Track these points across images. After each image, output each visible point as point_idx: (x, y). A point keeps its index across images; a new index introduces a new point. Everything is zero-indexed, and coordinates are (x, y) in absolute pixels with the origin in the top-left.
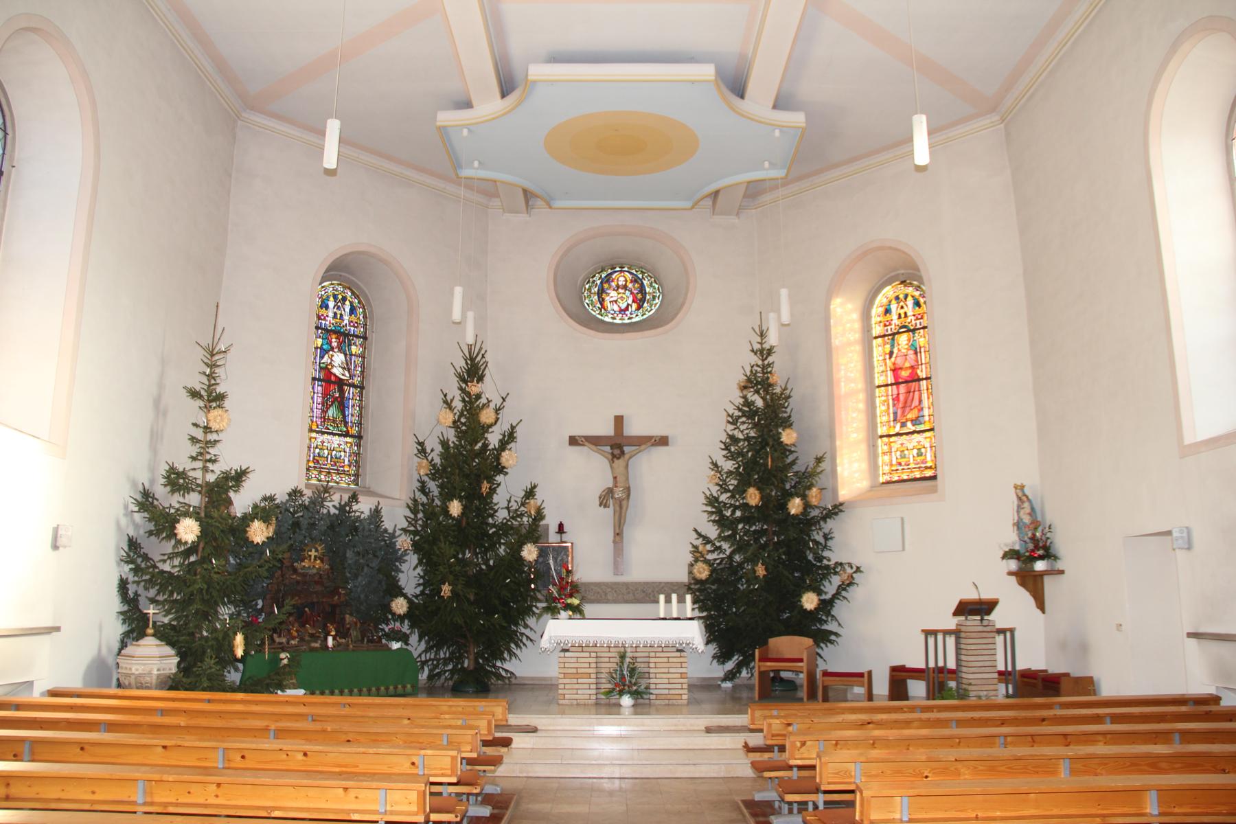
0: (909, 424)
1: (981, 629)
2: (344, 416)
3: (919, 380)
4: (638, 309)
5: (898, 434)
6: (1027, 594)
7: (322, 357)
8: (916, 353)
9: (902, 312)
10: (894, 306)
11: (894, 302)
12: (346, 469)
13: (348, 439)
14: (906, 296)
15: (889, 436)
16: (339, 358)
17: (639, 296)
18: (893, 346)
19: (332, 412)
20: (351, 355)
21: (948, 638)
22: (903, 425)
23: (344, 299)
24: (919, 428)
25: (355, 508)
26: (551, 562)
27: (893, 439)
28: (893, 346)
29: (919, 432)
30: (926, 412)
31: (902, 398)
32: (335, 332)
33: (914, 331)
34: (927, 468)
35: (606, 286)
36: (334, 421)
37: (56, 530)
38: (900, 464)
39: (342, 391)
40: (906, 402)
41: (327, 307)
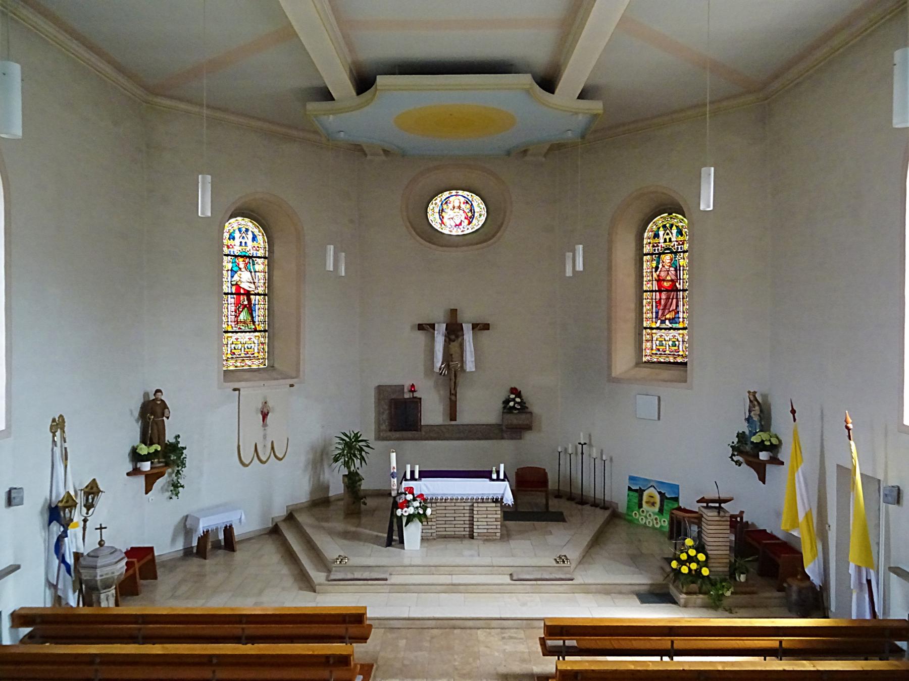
0: (667, 322)
1: (717, 518)
2: (252, 317)
3: (678, 290)
4: (470, 223)
5: (658, 328)
6: (753, 470)
7: (232, 277)
8: (676, 270)
9: (667, 237)
10: (661, 232)
11: (661, 229)
12: (256, 355)
13: (257, 334)
14: (672, 226)
15: (652, 329)
17: (470, 214)
18: (658, 263)
19: (243, 316)
22: (663, 322)
23: (247, 230)
24: (674, 326)
27: (654, 331)
28: (658, 263)
29: (675, 329)
30: (681, 315)
31: (663, 302)
32: (241, 257)
33: (676, 253)
35: (445, 207)
36: (244, 323)
37: (9, 492)
38: (659, 350)
39: (249, 300)
40: (665, 305)
41: (234, 238)
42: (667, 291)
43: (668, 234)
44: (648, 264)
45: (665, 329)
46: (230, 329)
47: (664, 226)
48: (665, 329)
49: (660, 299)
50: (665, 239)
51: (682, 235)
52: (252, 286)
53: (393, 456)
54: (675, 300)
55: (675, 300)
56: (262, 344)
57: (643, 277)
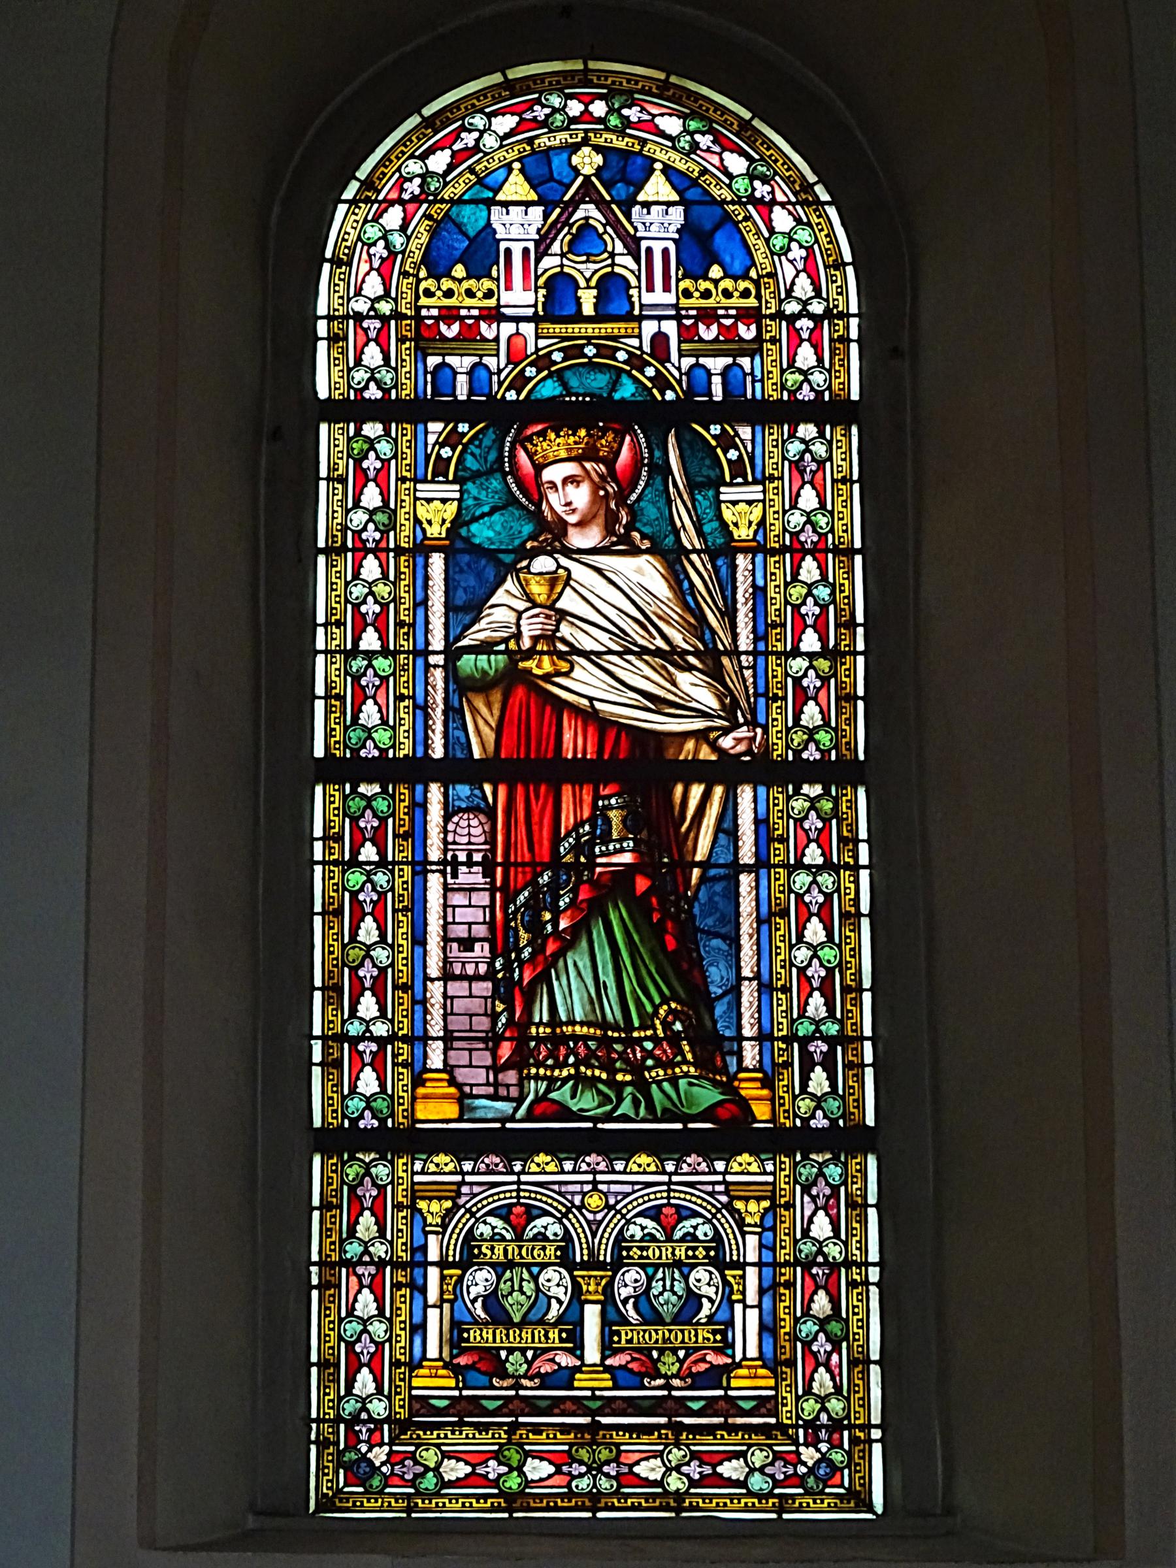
2: (695, 998)
7: (466, 607)
10: (517, 226)
12: (743, 1386)
13: (745, 1166)
16: (618, 588)
20: (724, 549)
25: (348, 1256)
39: (660, 831)
41: (482, 254)
46: (437, 1111)
50: (559, 288)
52: (696, 689)
56: (829, 1274)
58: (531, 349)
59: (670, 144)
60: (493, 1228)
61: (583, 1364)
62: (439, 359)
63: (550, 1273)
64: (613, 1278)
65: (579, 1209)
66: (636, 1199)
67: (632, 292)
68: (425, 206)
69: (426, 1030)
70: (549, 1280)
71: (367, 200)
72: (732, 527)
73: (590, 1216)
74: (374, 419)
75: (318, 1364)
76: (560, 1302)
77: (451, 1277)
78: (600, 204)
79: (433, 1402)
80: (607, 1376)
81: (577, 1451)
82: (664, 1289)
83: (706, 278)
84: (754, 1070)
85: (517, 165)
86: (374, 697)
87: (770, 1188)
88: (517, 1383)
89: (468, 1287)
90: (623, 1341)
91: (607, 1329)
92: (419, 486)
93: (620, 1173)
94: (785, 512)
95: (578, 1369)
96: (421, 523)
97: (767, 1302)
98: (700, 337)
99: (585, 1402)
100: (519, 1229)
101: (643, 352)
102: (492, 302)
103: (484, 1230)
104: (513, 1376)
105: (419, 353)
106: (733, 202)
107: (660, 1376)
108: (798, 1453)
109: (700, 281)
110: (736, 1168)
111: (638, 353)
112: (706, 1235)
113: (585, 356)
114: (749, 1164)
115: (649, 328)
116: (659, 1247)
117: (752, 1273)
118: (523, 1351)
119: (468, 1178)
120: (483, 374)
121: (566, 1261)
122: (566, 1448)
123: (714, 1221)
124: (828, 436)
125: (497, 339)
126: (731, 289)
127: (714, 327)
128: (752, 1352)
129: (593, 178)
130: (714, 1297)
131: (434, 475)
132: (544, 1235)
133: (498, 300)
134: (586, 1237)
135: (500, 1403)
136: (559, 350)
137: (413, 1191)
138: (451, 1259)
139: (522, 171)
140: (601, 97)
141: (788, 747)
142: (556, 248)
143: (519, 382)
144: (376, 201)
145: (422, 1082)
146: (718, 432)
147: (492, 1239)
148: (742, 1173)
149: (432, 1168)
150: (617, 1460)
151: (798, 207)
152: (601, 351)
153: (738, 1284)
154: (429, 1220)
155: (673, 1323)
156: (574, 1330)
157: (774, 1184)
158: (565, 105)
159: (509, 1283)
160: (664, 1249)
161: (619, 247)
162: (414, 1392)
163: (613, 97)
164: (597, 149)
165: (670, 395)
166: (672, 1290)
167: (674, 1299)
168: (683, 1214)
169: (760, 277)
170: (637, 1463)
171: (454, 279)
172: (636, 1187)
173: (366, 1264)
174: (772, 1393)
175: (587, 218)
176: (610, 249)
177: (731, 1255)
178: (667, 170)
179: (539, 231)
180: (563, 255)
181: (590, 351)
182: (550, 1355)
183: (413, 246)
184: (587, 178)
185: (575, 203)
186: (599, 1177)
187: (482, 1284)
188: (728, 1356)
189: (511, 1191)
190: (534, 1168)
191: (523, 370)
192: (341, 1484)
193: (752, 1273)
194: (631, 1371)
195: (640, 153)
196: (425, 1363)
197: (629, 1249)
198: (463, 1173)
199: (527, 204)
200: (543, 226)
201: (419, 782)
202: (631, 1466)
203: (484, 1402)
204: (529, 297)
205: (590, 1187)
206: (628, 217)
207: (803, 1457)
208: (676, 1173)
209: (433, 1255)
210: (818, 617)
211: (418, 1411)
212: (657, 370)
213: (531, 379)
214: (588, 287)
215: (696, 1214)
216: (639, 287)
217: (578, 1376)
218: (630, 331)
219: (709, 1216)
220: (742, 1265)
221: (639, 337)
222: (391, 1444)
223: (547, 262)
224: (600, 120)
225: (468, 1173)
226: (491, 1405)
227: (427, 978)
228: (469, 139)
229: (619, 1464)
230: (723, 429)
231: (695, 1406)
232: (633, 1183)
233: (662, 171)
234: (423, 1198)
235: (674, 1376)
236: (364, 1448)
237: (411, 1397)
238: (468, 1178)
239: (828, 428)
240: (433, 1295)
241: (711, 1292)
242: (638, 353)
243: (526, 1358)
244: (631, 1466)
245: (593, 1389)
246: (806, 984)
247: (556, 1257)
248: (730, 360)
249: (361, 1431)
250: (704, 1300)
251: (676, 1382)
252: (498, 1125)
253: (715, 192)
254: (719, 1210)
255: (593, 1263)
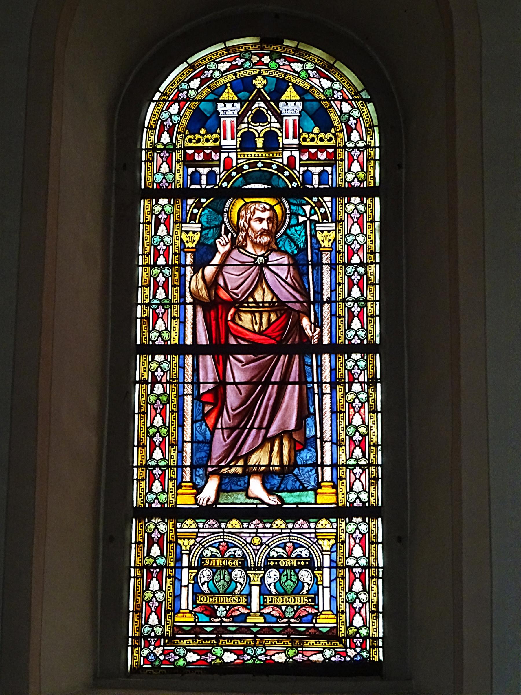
0: (256, 486)
3: (307, 348)
8: (297, 264)
10: (229, 112)
14: (281, 86)
15: (176, 514)
21: (175, 620)
26: (114, 179)
31: (232, 397)
33: (303, 193)
34: (317, 635)
38: (210, 611)
40: (246, 412)
42: (253, 348)
43: (259, 117)
44: (162, 233)
45: (246, 515)
47: (244, 86)
48: (246, 515)
49: (221, 384)
51: (326, 125)
53: (263, 380)
54: (292, 393)
55: (292, 393)
57: (132, 287)
58: (234, 164)
59: (297, 75)
60: (212, 552)
61: (251, 612)
62: (194, 169)
63: (236, 571)
64: (264, 574)
65: (250, 544)
66: (273, 541)
67: (279, 138)
68: (189, 103)
69: (183, 463)
70: (236, 575)
71: (164, 100)
72: (321, 242)
73: (254, 547)
74: (355, 196)
75: (133, 611)
76: (241, 585)
77: (192, 573)
78: (265, 101)
79: (184, 628)
80: (262, 618)
81: (247, 650)
82: (287, 579)
83: (199, 133)
84: (329, 482)
85: (229, 85)
86: (162, 318)
87: (335, 534)
88: (289, 621)
89: (200, 578)
90: (268, 602)
91: (262, 597)
92: (183, 225)
93: (246, 528)
94: (345, 236)
95: (248, 614)
96: (184, 243)
97: (334, 585)
98: (318, 158)
99: (251, 629)
100: (223, 553)
101: (284, 165)
102: (217, 144)
103: (208, 553)
104: (220, 617)
105: (185, 167)
106: (324, 100)
107: (285, 618)
108: (347, 652)
109: (196, 135)
110: (275, 526)
111: (282, 165)
112: (306, 555)
113: (258, 167)
114: (258, 524)
115: (286, 154)
116: (284, 561)
117: (326, 571)
118: (292, 607)
119: (201, 530)
120: (198, 175)
121: (244, 566)
122: (242, 648)
123: (243, 549)
124: (365, 202)
125: (219, 160)
126: (210, 138)
127: (202, 154)
128: (327, 607)
129: (262, 90)
130: (309, 582)
131: (190, 220)
132: (301, 555)
133: (220, 143)
134: (253, 557)
135: (281, 629)
136: (247, 164)
137: (177, 536)
138: (193, 565)
139: (231, 87)
140: (267, 55)
141: (345, 338)
142: (246, 120)
143: (228, 179)
144: (168, 100)
145: (320, 487)
146: (316, 201)
147: (211, 557)
148: (233, 528)
149: (207, 526)
150: (265, 654)
151: (353, 102)
152: (266, 165)
153: (320, 577)
154: (184, 548)
155: (292, 594)
156: (315, 598)
157: (337, 533)
158: (251, 58)
159: (286, 577)
160: (286, 561)
161: (274, 119)
162: (175, 624)
163: (273, 54)
164: (264, 77)
165: (294, 184)
166: (224, 579)
167: (292, 584)
168: (296, 546)
169: (336, 132)
170: (274, 655)
171: (201, 135)
172: (275, 535)
173: (357, 567)
174: (335, 625)
175: (259, 107)
176: (269, 120)
177: (318, 564)
178: (295, 86)
179: (238, 112)
180: (249, 123)
181: (260, 165)
182: (236, 608)
183: (183, 120)
184: (259, 89)
185: (253, 102)
186: (259, 531)
187: (273, 577)
188: (316, 609)
189: (220, 536)
190: (207, 526)
191: (231, 173)
192: (142, 664)
193: (326, 571)
194: (272, 615)
195: (237, 79)
196: (181, 611)
197: (270, 561)
198: (199, 528)
199: (234, 101)
200: (240, 110)
201: (182, 355)
202: (271, 656)
203: (274, 629)
204: (234, 142)
205: (254, 535)
206: (278, 106)
207: (348, 654)
208: (293, 528)
209: (185, 563)
210: (164, 282)
211: (177, 632)
212: (290, 173)
213: (234, 177)
214: (259, 137)
215: (236, 546)
216: (282, 136)
217: (248, 617)
218: (242, 156)
219: (241, 547)
220: (321, 568)
221: (282, 158)
222: (163, 647)
223: (243, 126)
224: (267, 65)
225: (201, 528)
226: (278, 630)
227: (184, 442)
228: (208, 74)
229: (266, 655)
230: (318, 200)
231: (278, 630)
232: (273, 533)
233: (293, 86)
234: (181, 539)
235: (224, 617)
236: (152, 648)
237: (174, 626)
238: (201, 530)
239: (365, 199)
240: (185, 582)
241: (241, 580)
242: (282, 165)
243: (294, 609)
244: (271, 656)
245: (255, 623)
246: (353, 443)
247: (239, 564)
248: (322, 168)
249: (151, 640)
250: (305, 584)
251: (292, 620)
252: (295, 506)
253: (317, 96)
254: (246, 545)
255: (256, 568)
